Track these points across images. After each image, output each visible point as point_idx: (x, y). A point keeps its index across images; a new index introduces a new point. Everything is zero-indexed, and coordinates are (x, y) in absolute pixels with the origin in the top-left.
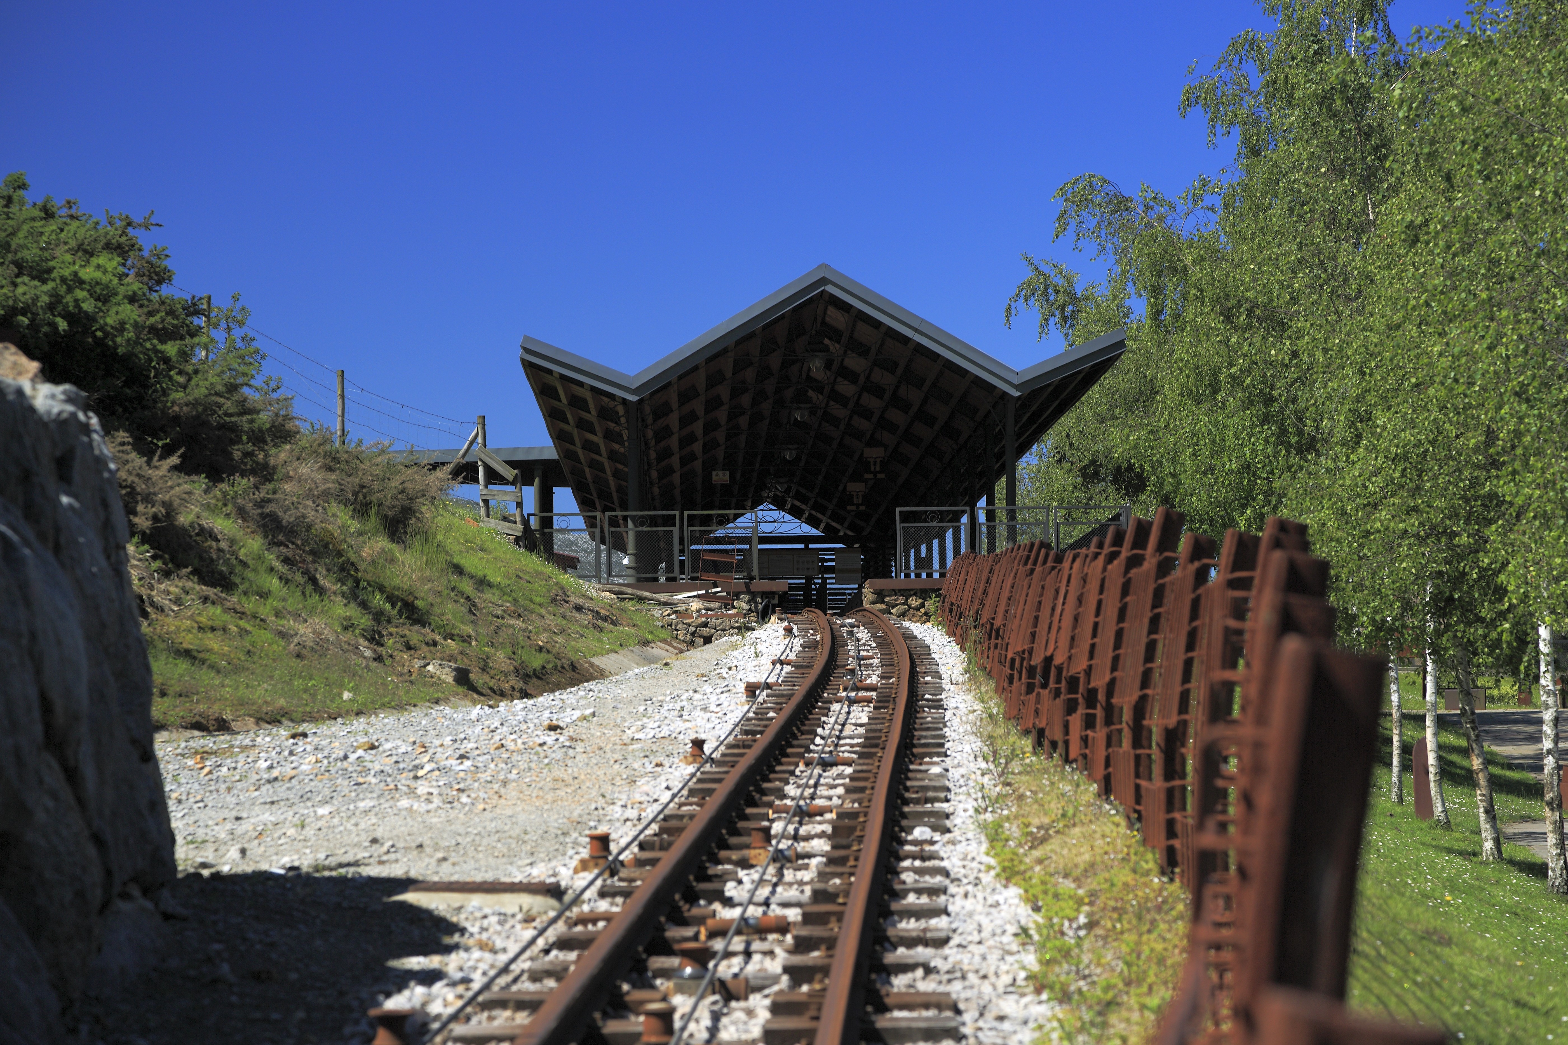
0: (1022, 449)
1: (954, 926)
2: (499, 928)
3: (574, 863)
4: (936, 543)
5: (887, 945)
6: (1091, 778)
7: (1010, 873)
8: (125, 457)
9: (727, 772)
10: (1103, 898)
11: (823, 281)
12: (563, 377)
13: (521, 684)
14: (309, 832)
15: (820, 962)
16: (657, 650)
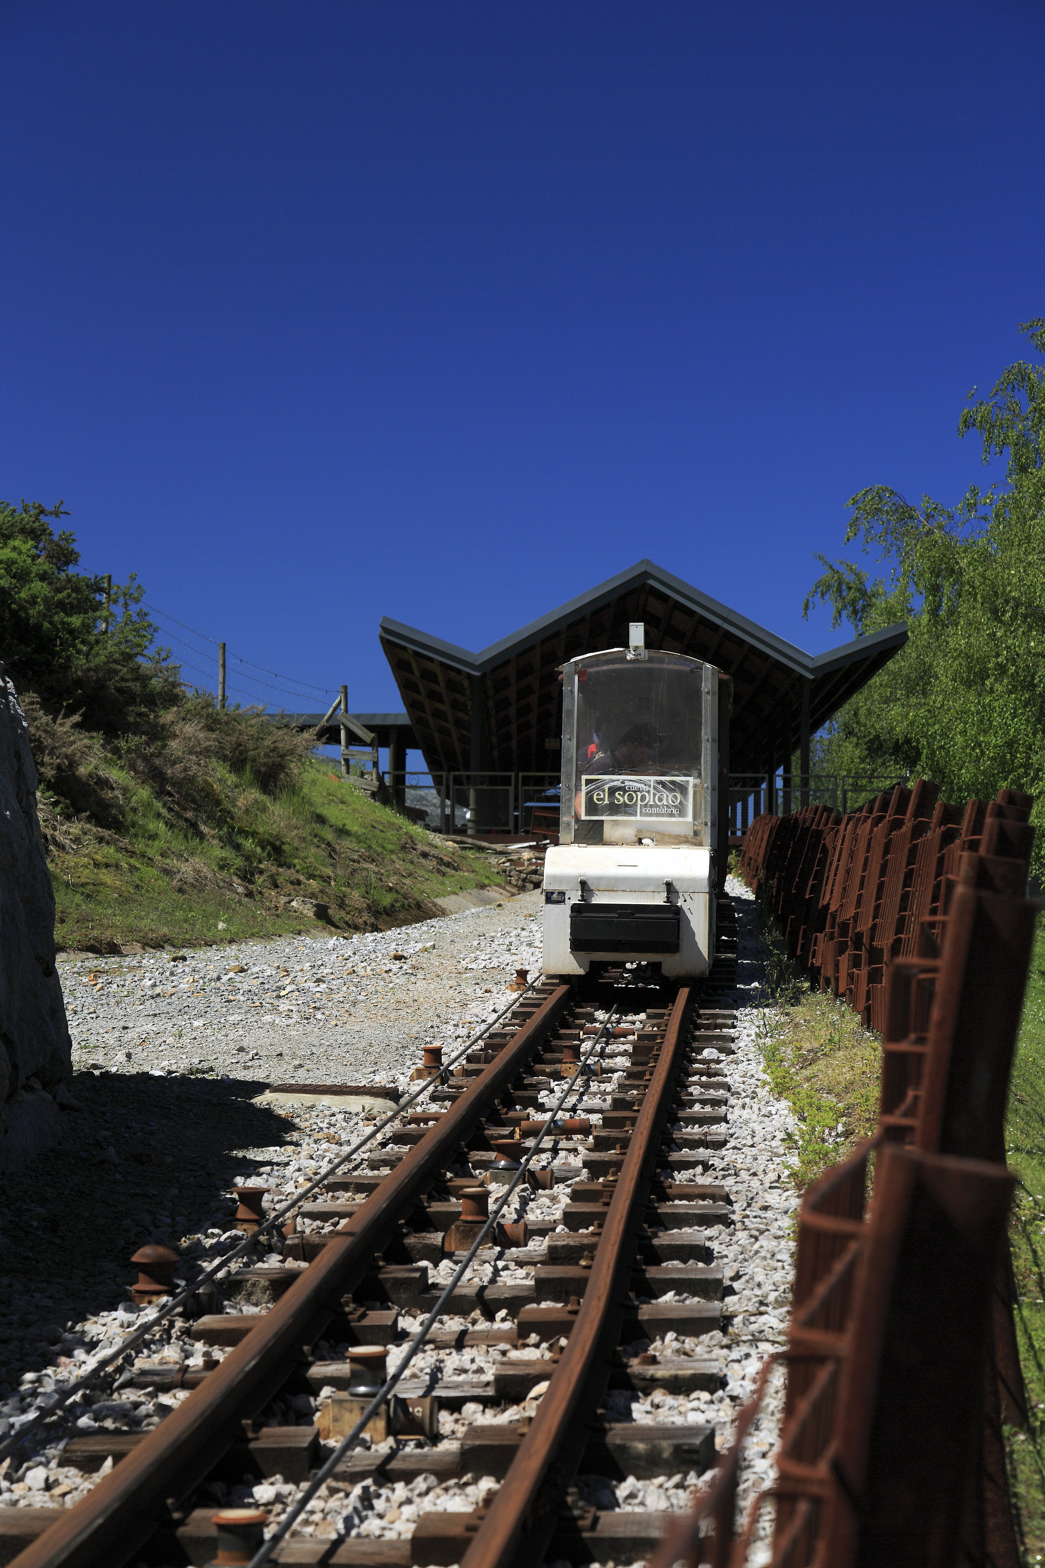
0: (816, 725)
1: (731, 1131)
2: (345, 1124)
3: (410, 1072)
4: (739, 805)
5: (673, 1146)
6: (855, 1009)
7: (781, 1089)
8: (35, 714)
9: (545, 999)
10: (858, 1111)
11: (646, 575)
12: (416, 653)
13: (373, 920)
14: (186, 1040)
15: (615, 1158)
16: (492, 893)
